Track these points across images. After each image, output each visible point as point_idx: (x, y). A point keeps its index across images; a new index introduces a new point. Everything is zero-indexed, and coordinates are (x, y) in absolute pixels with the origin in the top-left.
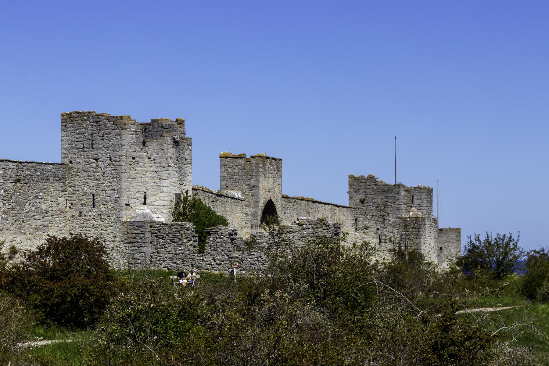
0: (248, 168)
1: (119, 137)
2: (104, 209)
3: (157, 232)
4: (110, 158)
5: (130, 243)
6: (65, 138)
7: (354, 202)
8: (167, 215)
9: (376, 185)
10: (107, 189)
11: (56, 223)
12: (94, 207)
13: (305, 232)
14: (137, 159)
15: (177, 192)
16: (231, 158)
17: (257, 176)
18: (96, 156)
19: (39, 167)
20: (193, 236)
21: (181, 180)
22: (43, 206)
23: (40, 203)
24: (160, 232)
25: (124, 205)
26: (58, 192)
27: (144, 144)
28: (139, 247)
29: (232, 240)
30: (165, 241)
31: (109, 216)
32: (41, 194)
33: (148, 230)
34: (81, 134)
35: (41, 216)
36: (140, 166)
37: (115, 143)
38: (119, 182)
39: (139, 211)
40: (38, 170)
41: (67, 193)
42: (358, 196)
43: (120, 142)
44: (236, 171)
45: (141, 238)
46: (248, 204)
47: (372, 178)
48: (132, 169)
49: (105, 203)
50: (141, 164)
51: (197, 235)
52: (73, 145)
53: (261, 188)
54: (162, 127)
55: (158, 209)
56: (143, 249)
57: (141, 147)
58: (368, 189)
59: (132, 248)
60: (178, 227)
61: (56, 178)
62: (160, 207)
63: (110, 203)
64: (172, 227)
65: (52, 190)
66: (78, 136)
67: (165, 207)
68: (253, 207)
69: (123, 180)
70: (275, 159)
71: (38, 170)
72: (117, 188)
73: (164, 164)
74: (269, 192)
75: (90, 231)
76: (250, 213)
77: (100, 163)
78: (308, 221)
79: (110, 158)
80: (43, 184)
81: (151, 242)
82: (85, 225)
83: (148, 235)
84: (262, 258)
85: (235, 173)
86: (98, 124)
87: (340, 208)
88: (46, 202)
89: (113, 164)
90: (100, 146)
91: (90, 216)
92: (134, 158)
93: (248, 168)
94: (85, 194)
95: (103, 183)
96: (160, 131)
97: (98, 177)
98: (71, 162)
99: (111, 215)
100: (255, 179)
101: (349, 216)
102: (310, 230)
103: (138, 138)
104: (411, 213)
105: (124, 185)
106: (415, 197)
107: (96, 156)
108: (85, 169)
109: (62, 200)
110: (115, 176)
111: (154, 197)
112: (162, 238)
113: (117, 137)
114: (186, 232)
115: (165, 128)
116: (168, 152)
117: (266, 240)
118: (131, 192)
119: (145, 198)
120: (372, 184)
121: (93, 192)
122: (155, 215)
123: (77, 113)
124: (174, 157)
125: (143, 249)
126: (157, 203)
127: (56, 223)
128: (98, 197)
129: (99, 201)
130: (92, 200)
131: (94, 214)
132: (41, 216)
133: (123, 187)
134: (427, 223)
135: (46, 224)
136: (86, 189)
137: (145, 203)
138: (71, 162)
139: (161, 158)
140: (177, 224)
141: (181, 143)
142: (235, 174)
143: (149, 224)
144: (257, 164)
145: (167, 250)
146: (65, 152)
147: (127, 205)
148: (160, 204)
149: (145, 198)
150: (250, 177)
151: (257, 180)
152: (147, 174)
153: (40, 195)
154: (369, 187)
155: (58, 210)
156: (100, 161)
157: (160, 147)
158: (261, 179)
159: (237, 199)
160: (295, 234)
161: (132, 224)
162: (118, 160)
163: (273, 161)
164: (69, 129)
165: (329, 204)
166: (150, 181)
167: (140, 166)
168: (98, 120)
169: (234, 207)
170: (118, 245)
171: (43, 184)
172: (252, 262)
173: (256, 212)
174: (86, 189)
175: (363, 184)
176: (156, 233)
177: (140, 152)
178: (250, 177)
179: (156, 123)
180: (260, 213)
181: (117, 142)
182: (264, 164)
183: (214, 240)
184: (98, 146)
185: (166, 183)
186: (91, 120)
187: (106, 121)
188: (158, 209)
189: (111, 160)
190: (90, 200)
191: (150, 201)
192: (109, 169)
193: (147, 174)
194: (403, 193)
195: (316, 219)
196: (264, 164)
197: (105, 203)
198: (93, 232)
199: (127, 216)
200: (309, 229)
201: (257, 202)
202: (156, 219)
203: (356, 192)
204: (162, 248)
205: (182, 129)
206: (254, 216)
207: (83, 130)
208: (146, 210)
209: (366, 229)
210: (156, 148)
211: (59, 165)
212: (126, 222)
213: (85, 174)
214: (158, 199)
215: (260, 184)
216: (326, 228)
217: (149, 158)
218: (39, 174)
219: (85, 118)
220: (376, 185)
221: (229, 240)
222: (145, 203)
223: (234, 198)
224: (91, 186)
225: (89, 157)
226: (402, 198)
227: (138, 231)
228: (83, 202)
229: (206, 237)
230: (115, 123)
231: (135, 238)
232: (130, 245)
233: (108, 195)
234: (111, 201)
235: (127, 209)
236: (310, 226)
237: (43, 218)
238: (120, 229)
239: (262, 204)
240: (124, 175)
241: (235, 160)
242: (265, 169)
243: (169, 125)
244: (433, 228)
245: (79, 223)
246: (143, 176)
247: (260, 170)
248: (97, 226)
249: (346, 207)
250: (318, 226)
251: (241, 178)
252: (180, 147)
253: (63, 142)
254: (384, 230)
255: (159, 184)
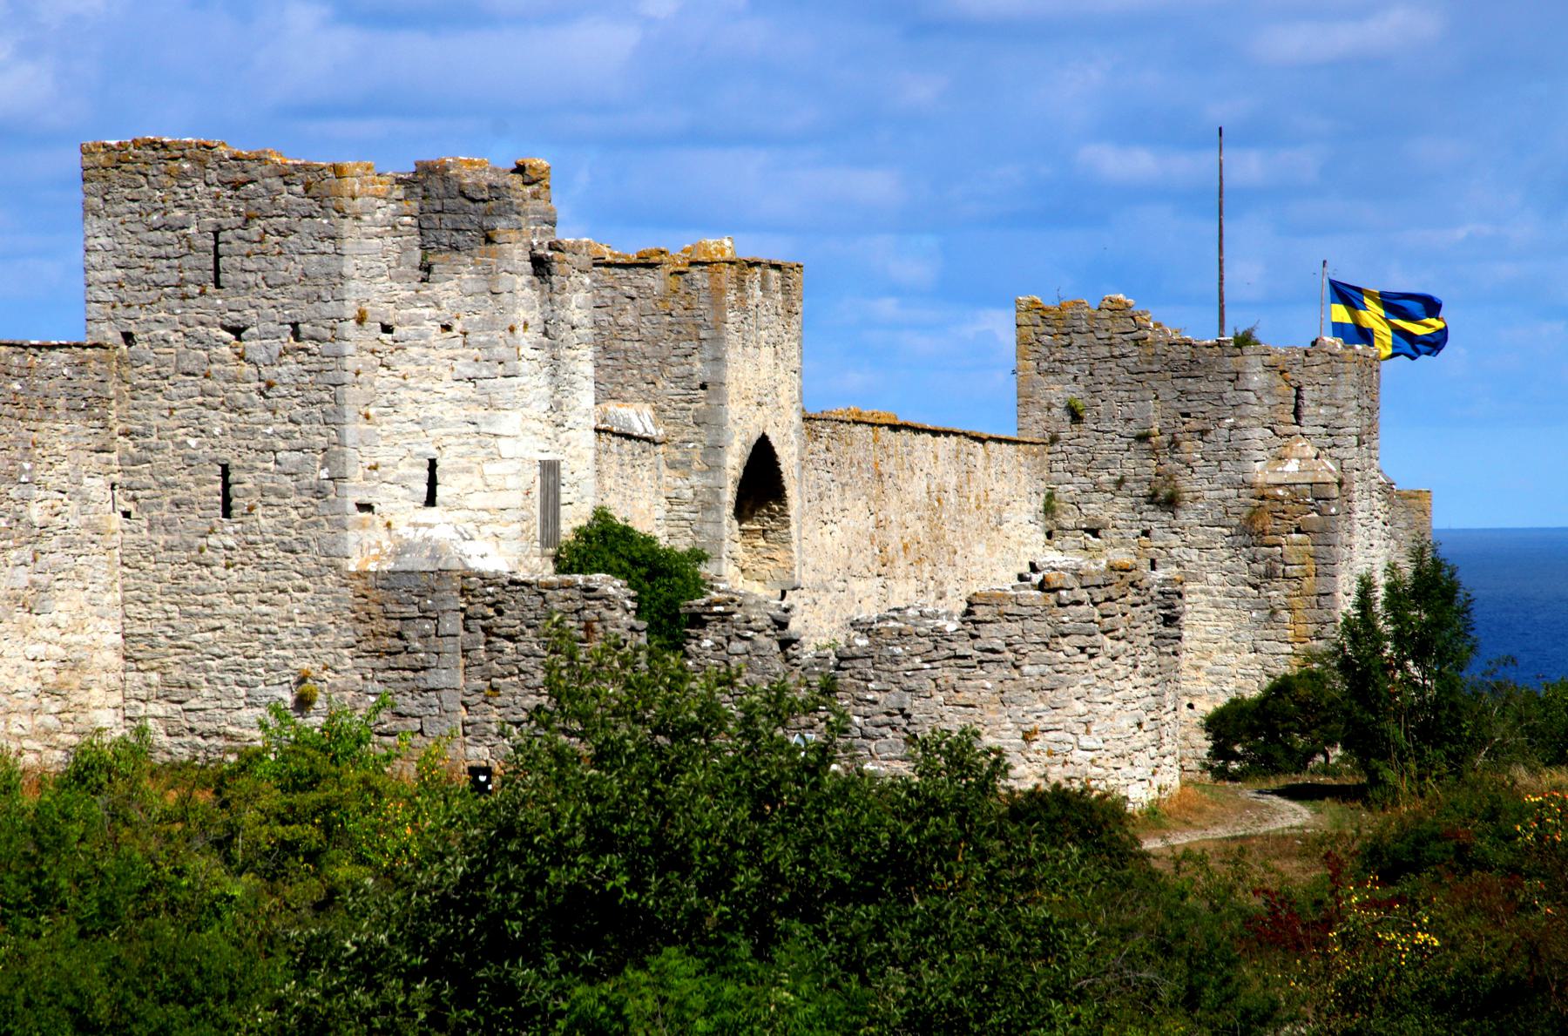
0: (679, 310)
1: (327, 246)
2: (272, 521)
3: (491, 612)
4: (295, 325)
5: (377, 653)
6: (103, 240)
7: (1038, 415)
8: (516, 545)
9: (1136, 341)
10: (281, 444)
11: (79, 576)
12: (227, 512)
13: (1067, 616)
14: (399, 332)
15: (545, 457)
16: (608, 265)
17: (718, 340)
18: (235, 315)
19: (16, 360)
20: (632, 629)
21: (559, 404)
22: (36, 513)
23: (24, 501)
24: (500, 613)
25: (351, 507)
26: (83, 455)
27: (427, 269)
28: (415, 670)
29: (785, 644)
30: (523, 647)
31: (292, 552)
32: (27, 466)
33: (453, 605)
34: (171, 228)
35: (27, 553)
36: (411, 360)
37: (313, 269)
38: (334, 419)
39: (390, 530)
40: (15, 371)
41: (114, 456)
42: (1059, 391)
43: (334, 265)
44: (627, 319)
45: (424, 636)
46: (678, 455)
47: (1119, 310)
48: (383, 371)
49: (273, 499)
50: (414, 351)
51: (645, 624)
52: (138, 273)
53: (732, 390)
54: (462, 194)
55: (480, 524)
56: (432, 679)
57: (415, 285)
58: (1104, 360)
59: (390, 674)
60: (576, 594)
61: (73, 403)
62: (485, 516)
63: (295, 500)
64: (550, 593)
65: (61, 448)
66: (156, 236)
67: (506, 515)
68: (701, 473)
69: (350, 413)
70: (777, 267)
71: (15, 371)
72: (321, 441)
73: (501, 351)
74: (760, 404)
75: (211, 605)
76: (689, 494)
77: (253, 343)
78: (1077, 574)
79: (295, 325)
80: (33, 425)
81: (465, 652)
82: (193, 583)
83: (452, 623)
84: (908, 716)
85: (624, 328)
86: (241, 193)
87: (992, 445)
88: (42, 494)
89: (305, 350)
90: (250, 278)
91: (214, 549)
92: (387, 329)
93: (679, 310)
94: (190, 462)
95: (267, 424)
96: (454, 212)
97: (242, 399)
98: (128, 338)
99: (299, 548)
100: (708, 355)
101: (1024, 479)
102: (1082, 609)
103: (404, 250)
104: (1292, 466)
105: (354, 429)
106: (1307, 393)
107: (235, 315)
108: (190, 368)
109: (96, 486)
110: (314, 396)
111: (465, 479)
112: (510, 638)
113: (322, 247)
114: (606, 613)
115: (473, 200)
116: (514, 305)
117: (922, 649)
118: (382, 454)
119: (432, 483)
120: (1117, 340)
121: (225, 455)
122: (468, 547)
123: (152, 144)
124: (535, 317)
125: (432, 679)
126: (476, 501)
127: (79, 576)
128: (245, 476)
129: (248, 492)
130: (219, 486)
131: (230, 542)
132: (27, 553)
133: (349, 441)
134: (1357, 506)
135: (42, 580)
136: (192, 442)
137: (431, 500)
138: (128, 338)
139: (491, 324)
140: (571, 586)
141: (556, 267)
142: (626, 334)
143: (457, 584)
144: (716, 294)
145: (531, 683)
146: (102, 296)
147: (366, 507)
148: (489, 504)
149: (432, 483)
150: (686, 346)
151: (718, 360)
152: (438, 387)
153: (23, 471)
154: (1105, 351)
155: (86, 526)
156: (252, 337)
157: (485, 285)
158: (732, 354)
159: (638, 439)
160: (1030, 623)
161: (388, 581)
162: (328, 334)
163: (774, 273)
164: (119, 209)
165: (947, 433)
166: (447, 417)
167: (411, 360)
168: (240, 176)
169: (630, 471)
170: (330, 659)
171: (33, 425)
172: (870, 730)
173: (716, 492)
174: (192, 442)
175: (1078, 340)
176: (485, 618)
177: (410, 302)
178: (686, 346)
179: (435, 179)
180: (729, 495)
181: (321, 264)
182: (741, 288)
183: (719, 646)
184: (241, 276)
185: (508, 422)
186: (212, 176)
187: (277, 183)
188: (480, 524)
189: (296, 334)
190: (209, 488)
191: (450, 491)
192: (291, 365)
193: (438, 387)
194: (1257, 378)
195: (1104, 563)
196: (741, 288)
197: (273, 499)
198: (224, 609)
199: (366, 549)
200: (1079, 603)
201: (716, 448)
202: (476, 564)
203: (1048, 372)
204: (511, 674)
205: (541, 205)
206: (707, 507)
207: (179, 213)
208: (440, 526)
209: (1095, 533)
210: (470, 287)
211: (84, 347)
212: (361, 575)
213: (191, 385)
214: (479, 484)
215: (730, 375)
216: (1138, 599)
217: (447, 328)
218: (16, 386)
219: (186, 166)
220: (1136, 341)
221: (776, 647)
222: (431, 500)
223: (629, 437)
224: (217, 431)
225: (205, 318)
226: (1251, 396)
227: (413, 611)
228: (180, 494)
229: (688, 635)
230: (313, 192)
231: (400, 636)
232: (380, 663)
233: (286, 468)
234: (299, 491)
235: (362, 525)
236: (1084, 595)
237: (35, 560)
238: (336, 600)
239: (734, 461)
240: (351, 393)
241: (623, 273)
242: (746, 311)
243: (490, 187)
244: (1378, 524)
245: (167, 575)
246: (423, 397)
247: (730, 315)
248: (242, 586)
249: (1008, 441)
250: (1113, 591)
251: (648, 350)
252: (554, 278)
253: (94, 259)
254: (1175, 540)
255: (484, 429)
